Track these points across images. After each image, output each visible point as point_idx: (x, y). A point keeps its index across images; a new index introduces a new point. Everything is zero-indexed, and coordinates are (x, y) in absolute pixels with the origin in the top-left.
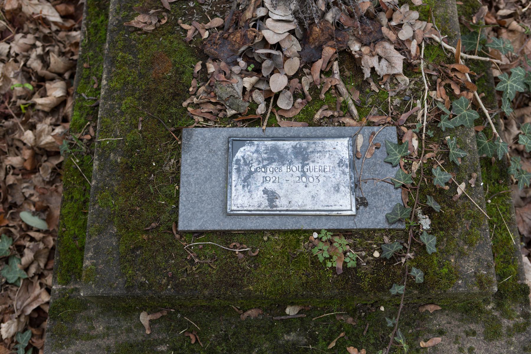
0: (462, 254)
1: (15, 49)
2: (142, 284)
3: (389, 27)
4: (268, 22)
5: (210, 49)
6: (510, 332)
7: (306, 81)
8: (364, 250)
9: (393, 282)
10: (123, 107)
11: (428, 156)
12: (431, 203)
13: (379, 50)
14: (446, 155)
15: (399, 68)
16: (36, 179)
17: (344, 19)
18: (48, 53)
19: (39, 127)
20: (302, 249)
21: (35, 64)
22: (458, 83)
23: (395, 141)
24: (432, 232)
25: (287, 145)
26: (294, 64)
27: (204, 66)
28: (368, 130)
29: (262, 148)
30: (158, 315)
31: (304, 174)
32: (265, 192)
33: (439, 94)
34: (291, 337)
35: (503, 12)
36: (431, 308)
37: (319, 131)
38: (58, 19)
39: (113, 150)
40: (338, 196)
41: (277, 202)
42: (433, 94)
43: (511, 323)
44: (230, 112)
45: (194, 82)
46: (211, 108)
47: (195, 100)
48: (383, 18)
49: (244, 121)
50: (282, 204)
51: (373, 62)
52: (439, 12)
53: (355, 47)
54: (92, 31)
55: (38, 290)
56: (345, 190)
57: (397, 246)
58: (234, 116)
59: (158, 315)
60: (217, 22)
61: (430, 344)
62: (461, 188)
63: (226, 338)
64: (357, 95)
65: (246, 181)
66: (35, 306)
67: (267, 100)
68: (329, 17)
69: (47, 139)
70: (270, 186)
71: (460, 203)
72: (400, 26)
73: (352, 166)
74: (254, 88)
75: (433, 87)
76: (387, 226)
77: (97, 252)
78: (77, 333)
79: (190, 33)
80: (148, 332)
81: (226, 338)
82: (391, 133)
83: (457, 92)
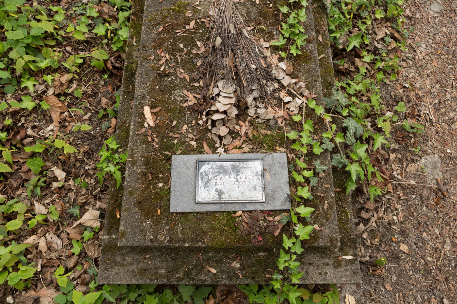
32: (217, 190)
40: (255, 192)
41: (223, 196)
50: (225, 197)
65: (206, 184)
70: (219, 187)
73: (263, 175)
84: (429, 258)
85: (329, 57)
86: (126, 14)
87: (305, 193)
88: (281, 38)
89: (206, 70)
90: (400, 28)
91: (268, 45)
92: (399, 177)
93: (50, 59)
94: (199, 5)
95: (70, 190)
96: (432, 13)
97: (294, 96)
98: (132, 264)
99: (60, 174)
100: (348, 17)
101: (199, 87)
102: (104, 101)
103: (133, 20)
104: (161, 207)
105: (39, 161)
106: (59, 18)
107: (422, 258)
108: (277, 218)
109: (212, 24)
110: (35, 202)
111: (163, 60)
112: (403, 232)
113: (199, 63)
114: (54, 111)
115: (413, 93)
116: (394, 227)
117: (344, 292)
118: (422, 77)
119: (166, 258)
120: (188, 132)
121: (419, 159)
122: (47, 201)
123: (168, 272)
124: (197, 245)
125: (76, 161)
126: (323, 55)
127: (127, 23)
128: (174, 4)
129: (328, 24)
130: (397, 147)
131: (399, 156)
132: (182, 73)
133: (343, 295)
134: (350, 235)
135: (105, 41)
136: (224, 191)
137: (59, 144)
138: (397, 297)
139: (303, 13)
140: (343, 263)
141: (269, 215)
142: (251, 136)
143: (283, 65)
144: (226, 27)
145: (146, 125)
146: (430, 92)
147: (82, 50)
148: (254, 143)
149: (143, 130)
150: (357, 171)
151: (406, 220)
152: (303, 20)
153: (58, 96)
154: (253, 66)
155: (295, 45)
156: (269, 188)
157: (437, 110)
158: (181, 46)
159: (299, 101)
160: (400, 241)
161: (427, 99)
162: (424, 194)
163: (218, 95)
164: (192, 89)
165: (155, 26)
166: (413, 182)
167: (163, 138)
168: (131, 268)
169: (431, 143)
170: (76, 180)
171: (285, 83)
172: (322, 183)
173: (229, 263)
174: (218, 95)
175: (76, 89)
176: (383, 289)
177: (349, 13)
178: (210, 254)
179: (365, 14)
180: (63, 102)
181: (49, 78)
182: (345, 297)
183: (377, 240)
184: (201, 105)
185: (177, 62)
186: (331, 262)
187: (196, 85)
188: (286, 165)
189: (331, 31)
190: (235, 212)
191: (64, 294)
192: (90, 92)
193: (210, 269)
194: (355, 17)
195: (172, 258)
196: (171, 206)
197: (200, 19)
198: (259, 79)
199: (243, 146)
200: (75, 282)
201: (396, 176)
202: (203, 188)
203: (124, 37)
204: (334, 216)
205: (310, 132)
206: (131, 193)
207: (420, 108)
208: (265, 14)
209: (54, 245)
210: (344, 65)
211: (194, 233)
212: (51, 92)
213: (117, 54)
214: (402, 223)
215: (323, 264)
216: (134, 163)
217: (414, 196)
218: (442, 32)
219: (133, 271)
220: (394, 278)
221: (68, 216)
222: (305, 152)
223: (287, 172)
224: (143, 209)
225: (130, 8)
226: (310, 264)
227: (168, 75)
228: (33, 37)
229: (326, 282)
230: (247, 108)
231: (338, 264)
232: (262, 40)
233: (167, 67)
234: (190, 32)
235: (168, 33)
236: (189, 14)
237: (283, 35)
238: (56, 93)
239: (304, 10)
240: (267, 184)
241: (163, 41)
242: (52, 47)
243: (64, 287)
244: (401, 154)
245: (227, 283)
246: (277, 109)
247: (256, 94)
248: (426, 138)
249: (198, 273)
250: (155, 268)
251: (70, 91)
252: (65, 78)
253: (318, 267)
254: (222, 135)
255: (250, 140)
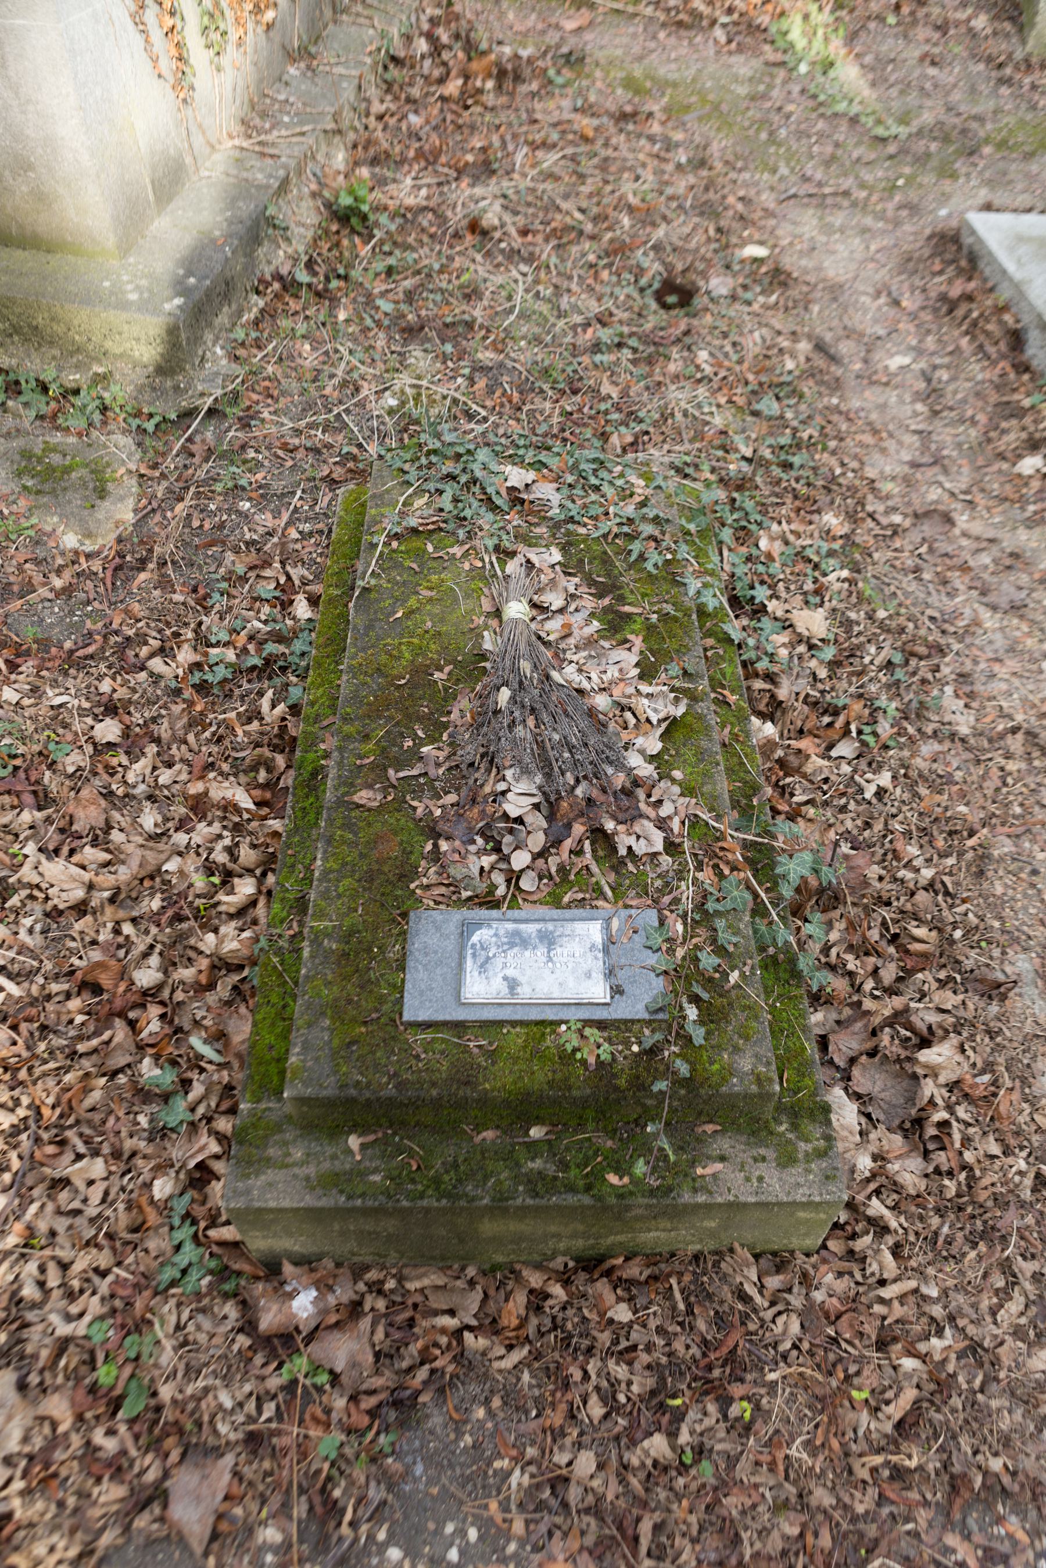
0: (736, 1050)
1: (197, 839)
2: (358, 1082)
3: (648, 804)
4: (509, 795)
5: (441, 826)
6: (808, 1158)
7: (553, 863)
8: (621, 1043)
9: (655, 1078)
10: (341, 890)
11: (694, 941)
12: (697, 989)
13: (637, 828)
14: (714, 941)
15: (659, 846)
16: (211, 998)
17: (595, 793)
18: (237, 844)
19: (223, 930)
20: (548, 1043)
21: (220, 857)
22: (728, 863)
23: (656, 924)
24: (701, 1022)
25: (531, 929)
26: (537, 841)
27: (436, 846)
28: (624, 913)
29: (502, 932)
30: (371, 1138)
31: (550, 959)
32: (505, 978)
33: (706, 876)
34: (537, 1164)
35: (799, 798)
36: (710, 1128)
37: (568, 913)
38: (251, 806)
39: (328, 935)
40: (590, 983)
41: (519, 990)
42: (700, 875)
43: (809, 1147)
44: (465, 894)
45: (423, 863)
46: (443, 890)
47: (425, 881)
48: (641, 794)
49: (481, 905)
50: (525, 992)
51: (631, 841)
52: (706, 789)
53: (610, 825)
54: (299, 814)
55: (204, 1138)
56: (598, 977)
57: (658, 1036)
58: (470, 899)
59: (371, 1138)
60: (452, 798)
61: (708, 1171)
62: (734, 977)
63: (455, 1166)
64: (612, 877)
65: (483, 967)
66: (199, 1158)
67: (508, 881)
68: (579, 791)
69: (231, 946)
70: (510, 972)
71: (733, 993)
72: (660, 802)
73: (606, 951)
74: (493, 868)
75: (699, 868)
76: (647, 1016)
77: (306, 1047)
78: (268, 1159)
79: (420, 811)
80: (358, 1158)
81: (455, 1166)
82: (651, 917)
83: (727, 872)
136: (522, 979)
196: (406, 1007)
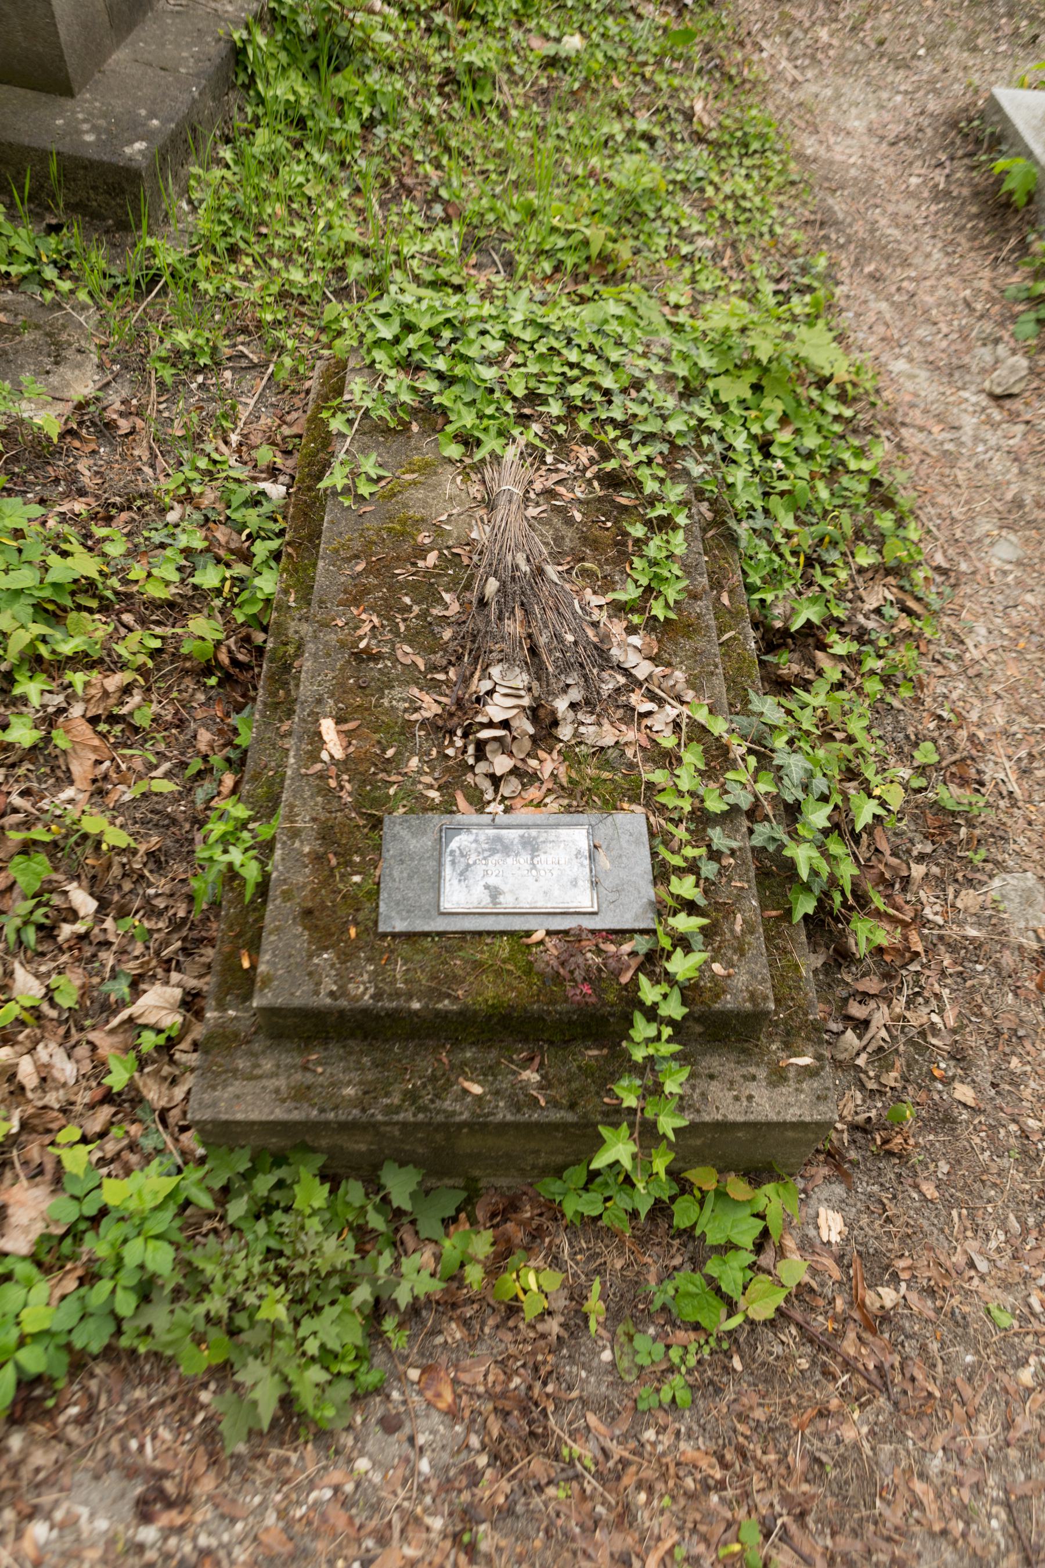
32: (487, 887)
41: (501, 899)
50: (507, 902)
70: (492, 881)
73: (592, 858)
84: (1031, 1122)
85: (746, 638)
86: (274, 544)
87: (686, 887)
88: (630, 585)
89: (463, 647)
90: (920, 592)
91: (602, 601)
92: (939, 920)
93: (84, 638)
94: (448, 521)
95: (107, 944)
96: (997, 563)
97: (660, 702)
98: (274, 1075)
99: (83, 901)
100: (793, 560)
101: (447, 682)
102: (205, 737)
103: (289, 555)
104: (357, 924)
105: (41, 863)
106: (116, 549)
107: (1014, 1121)
108: (627, 948)
109: (475, 558)
110: (17, 965)
111: (366, 628)
112: (959, 1056)
113: (447, 634)
114: (78, 757)
115: (963, 733)
116: (934, 1041)
117: (813, 1202)
118: (983, 699)
119: (358, 1062)
120: (420, 772)
121: (985, 878)
122: (43, 969)
123: (365, 1093)
124: (440, 1006)
125: (124, 875)
126: (732, 633)
127: (273, 564)
128: (391, 519)
129: (744, 572)
130: (929, 849)
131: (935, 870)
132: (406, 653)
133: (811, 1212)
134: (806, 1014)
135: (218, 603)
137: (93, 824)
138: (956, 1219)
139: (679, 537)
140: (791, 1075)
141: (606, 940)
142: (564, 781)
143: (635, 640)
144: (509, 558)
145: (325, 756)
146: (1005, 733)
147: (158, 623)
148: (571, 795)
149: (319, 766)
150: (810, 858)
151: (963, 1027)
152: (677, 552)
153: (94, 721)
154: (570, 638)
155: (661, 599)
156: (607, 883)
157: (1025, 773)
158: (407, 600)
159: (671, 712)
160: (953, 1078)
161: (999, 747)
162: (1003, 961)
163: (490, 693)
164: (434, 686)
165: (348, 560)
166: (972, 932)
167: (364, 783)
168: (271, 1084)
169: (1016, 847)
170: (121, 922)
171: (640, 674)
172: (730, 880)
173: (514, 1073)
174: (490, 693)
175: (139, 707)
176: (915, 1195)
177: (794, 553)
178: (468, 1055)
179: (833, 557)
180: (103, 736)
181: (78, 679)
182: (817, 1216)
183: (894, 1074)
184: (451, 715)
185: (397, 634)
186: (762, 1073)
187: (441, 677)
188: (645, 838)
189: (750, 589)
190: (528, 934)
191: (74, 1197)
192: (169, 718)
193: (467, 1085)
194: (810, 563)
195: (373, 1062)
197: (448, 548)
198: (581, 665)
199: (547, 800)
200: (104, 1171)
201: (931, 917)
202: (455, 882)
203: (267, 591)
204: (758, 947)
205: (697, 770)
206: (287, 896)
207: (982, 766)
208: (595, 541)
209: (56, 1073)
210: (788, 664)
211: (433, 978)
212: (77, 710)
213: (244, 631)
214: (954, 1031)
215: (744, 1076)
216: (295, 834)
217: (979, 968)
218: (1024, 603)
219: (277, 1091)
220: (944, 1167)
221: (96, 1006)
222: (688, 808)
223: (648, 853)
224: (313, 928)
225: (281, 533)
226: (712, 1077)
227: (376, 658)
228: (54, 585)
229: (752, 1118)
230: (555, 723)
231: (778, 1076)
232: (589, 591)
233: (374, 642)
234: (427, 573)
235: (378, 574)
236: (424, 538)
237: (636, 581)
238: (89, 714)
239: (680, 535)
240: (601, 876)
241: (366, 591)
242: (90, 611)
243: (75, 1177)
244: (938, 865)
245: (509, 1117)
246: (623, 728)
247: (575, 695)
248: (1001, 833)
249: (437, 1096)
250: (333, 1084)
251: (125, 710)
252: (115, 681)
253: (732, 1083)
254: (498, 773)
255: (563, 788)
